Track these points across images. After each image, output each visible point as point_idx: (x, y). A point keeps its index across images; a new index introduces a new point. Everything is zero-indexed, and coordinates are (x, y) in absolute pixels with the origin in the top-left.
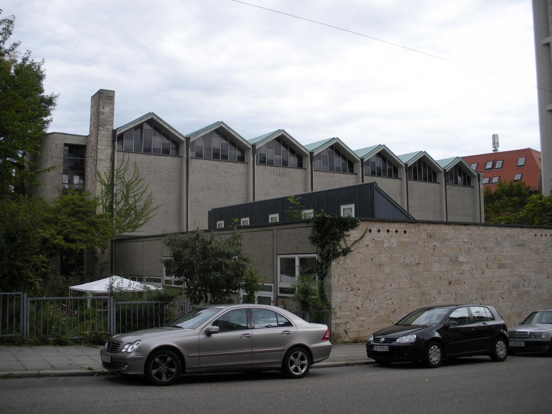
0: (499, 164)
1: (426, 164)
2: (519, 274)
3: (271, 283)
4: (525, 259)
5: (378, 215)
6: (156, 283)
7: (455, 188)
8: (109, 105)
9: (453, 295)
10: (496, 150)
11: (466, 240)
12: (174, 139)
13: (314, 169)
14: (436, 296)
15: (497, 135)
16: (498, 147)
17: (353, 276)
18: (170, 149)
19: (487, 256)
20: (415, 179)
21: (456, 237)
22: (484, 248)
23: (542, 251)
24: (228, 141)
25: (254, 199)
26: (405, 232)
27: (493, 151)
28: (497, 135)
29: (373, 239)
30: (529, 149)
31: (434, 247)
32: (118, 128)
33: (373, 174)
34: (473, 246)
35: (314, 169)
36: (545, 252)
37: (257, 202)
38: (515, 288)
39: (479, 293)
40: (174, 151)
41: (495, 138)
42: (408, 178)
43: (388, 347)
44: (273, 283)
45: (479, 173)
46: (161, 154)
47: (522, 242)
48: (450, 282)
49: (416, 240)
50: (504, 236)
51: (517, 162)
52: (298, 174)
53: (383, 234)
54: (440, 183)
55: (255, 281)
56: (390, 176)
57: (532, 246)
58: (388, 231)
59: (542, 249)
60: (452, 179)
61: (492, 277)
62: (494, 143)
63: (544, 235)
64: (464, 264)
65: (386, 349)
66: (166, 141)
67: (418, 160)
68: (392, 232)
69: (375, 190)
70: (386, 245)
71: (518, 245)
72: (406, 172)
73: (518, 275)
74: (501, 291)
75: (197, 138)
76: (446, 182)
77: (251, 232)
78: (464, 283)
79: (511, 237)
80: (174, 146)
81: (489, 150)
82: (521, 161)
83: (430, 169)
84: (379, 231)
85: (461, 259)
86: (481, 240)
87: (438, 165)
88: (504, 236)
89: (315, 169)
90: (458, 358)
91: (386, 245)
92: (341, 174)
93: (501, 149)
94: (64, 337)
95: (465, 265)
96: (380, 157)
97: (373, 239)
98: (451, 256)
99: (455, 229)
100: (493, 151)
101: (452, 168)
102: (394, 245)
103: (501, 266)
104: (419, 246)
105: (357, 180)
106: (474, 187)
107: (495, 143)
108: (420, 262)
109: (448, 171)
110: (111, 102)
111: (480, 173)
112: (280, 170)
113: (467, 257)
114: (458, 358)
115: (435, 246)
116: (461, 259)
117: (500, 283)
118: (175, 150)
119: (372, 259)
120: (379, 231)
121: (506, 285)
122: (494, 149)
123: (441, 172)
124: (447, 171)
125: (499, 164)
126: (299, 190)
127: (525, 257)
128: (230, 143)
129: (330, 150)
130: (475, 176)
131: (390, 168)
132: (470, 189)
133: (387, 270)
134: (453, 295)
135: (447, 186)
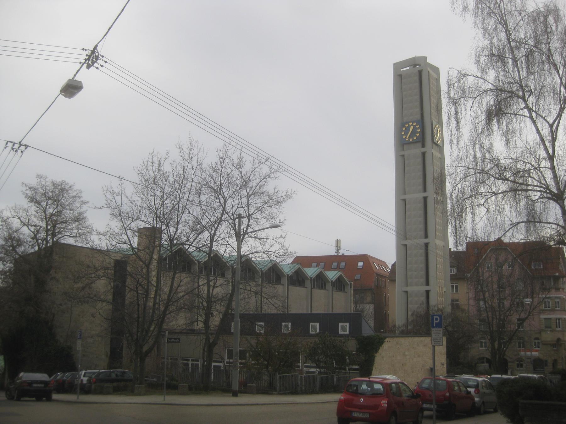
0: (343, 264)
25: (311, 312)
27: (336, 252)
37: (313, 314)
41: (338, 242)
42: (313, 286)
56: (300, 286)
62: (337, 247)
72: (332, 286)
82: (360, 264)
90: (402, 70)
93: (341, 252)
94: (424, 308)
103: (419, 356)
107: (338, 248)
114: (402, 70)
123: (329, 282)
125: (343, 264)
130: (348, 285)
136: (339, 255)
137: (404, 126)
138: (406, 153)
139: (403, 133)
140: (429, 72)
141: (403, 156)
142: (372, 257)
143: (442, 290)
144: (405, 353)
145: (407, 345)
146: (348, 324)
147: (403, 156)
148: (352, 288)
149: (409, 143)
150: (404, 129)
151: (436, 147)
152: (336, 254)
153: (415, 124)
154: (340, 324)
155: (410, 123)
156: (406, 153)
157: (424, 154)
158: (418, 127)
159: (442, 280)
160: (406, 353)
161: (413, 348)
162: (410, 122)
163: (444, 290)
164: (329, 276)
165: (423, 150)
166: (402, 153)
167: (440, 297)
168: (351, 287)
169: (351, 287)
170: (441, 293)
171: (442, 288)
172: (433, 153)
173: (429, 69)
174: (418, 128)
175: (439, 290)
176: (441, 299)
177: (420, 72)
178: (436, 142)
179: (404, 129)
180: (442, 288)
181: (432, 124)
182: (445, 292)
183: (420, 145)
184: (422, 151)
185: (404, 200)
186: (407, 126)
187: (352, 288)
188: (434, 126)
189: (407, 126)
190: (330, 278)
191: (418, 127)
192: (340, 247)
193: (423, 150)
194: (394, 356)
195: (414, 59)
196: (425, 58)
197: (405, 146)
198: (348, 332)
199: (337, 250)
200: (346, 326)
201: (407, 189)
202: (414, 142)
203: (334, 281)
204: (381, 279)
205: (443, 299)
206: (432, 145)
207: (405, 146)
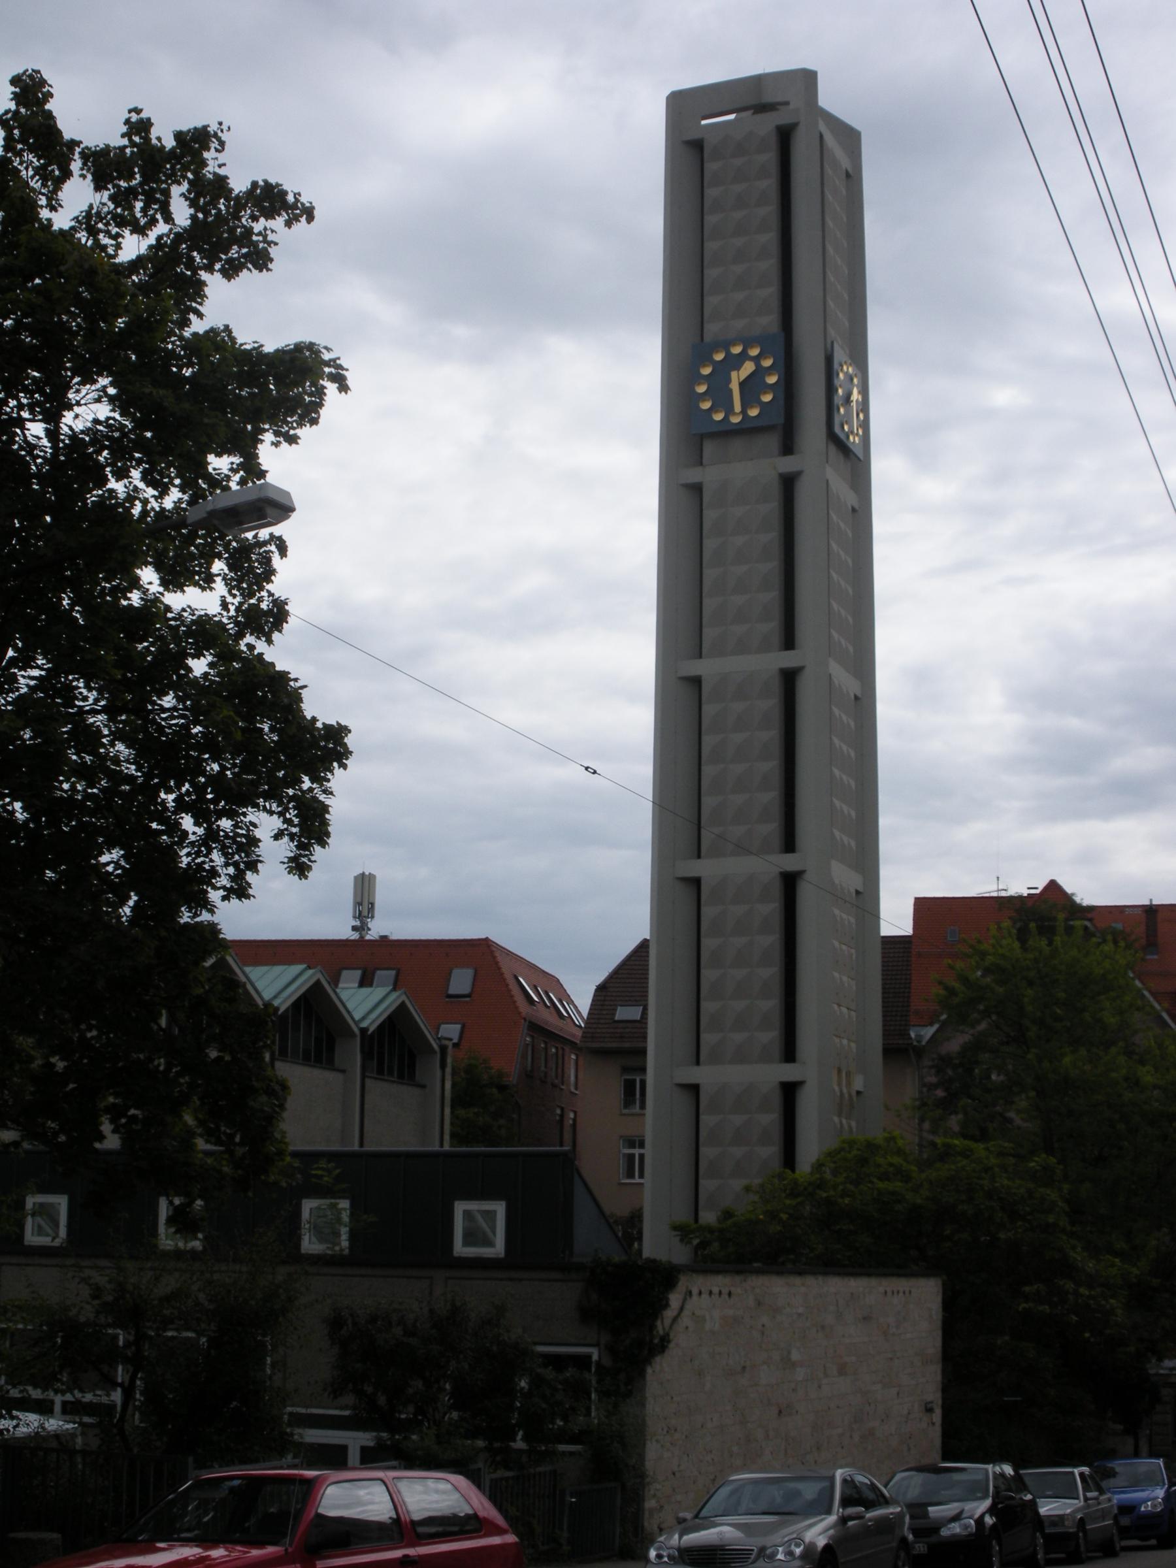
15: (372, 878)
16: (373, 917)
27: (354, 928)
28: (372, 878)
30: (487, 940)
43: (926, 1546)
51: (614, 1014)
62: (358, 903)
65: (922, 1549)
75: (282, 999)
76: (364, 1068)
77: (501, 1280)
87: (349, 1012)
93: (377, 928)
100: (354, 928)
103: (842, 1371)
106: (423, 1087)
107: (364, 906)
109: (374, 1032)
114: (704, 122)
122: (358, 923)
136: (368, 937)
137: (706, 359)
138: (709, 476)
139: (701, 389)
140: (821, 136)
141: (697, 489)
142: (509, 953)
143: (849, 1084)
144: (789, 1353)
145: (800, 1315)
146: (499, 1208)
147: (697, 489)
148: (448, 1070)
149: (727, 433)
150: (706, 371)
151: (841, 457)
152: (355, 936)
153: (754, 352)
154: (460, 1208)
155: (734, 345)
156: (709, 476)
157: (789, 483)
158: (767, 363)
159: (849, 1040)
160: (795, 1356)
161: (823, 1327)
162: (733, 343)
163: (858, 1083)
164: (350, 1006)
165: (787, 464)
166: (693, 475)
167: (840, 1115)
168: (443, 1066)
169: (443, 1066)
170: (846, 1096)
171: (848, 1074)
172: (827, 481)
173: (822, 127)
174: (769, 371)
175: (839, 1084)
176: (844, 1121)
177: (785, 136)
178: (842, 436)
179: (706, 371)
180: (848, 1074)
181: (829, 360)
182: (858, 1093)
183: (773, 442)
184: (780, 471)
185: (696, 682)
186: (719, 357)
187: (448, 1070)
188: (836, 366)
189: (719, 357)
190: (357, 1017)
191: (767, 363)
192: (373, 904)
193: (787, 464)
194: (744, 1368)
195: (757, 82)
196: (807, 79)
197: (709, 447)
198: (498, 1248)
199: (360, 916)
200: (490, 1216)
201: (709, 633)
202: (748, 430)
203: (372, 1029)
204: (546, 1049)
205: (853, 1124)
206: (827, 447)
207: (709, 447)
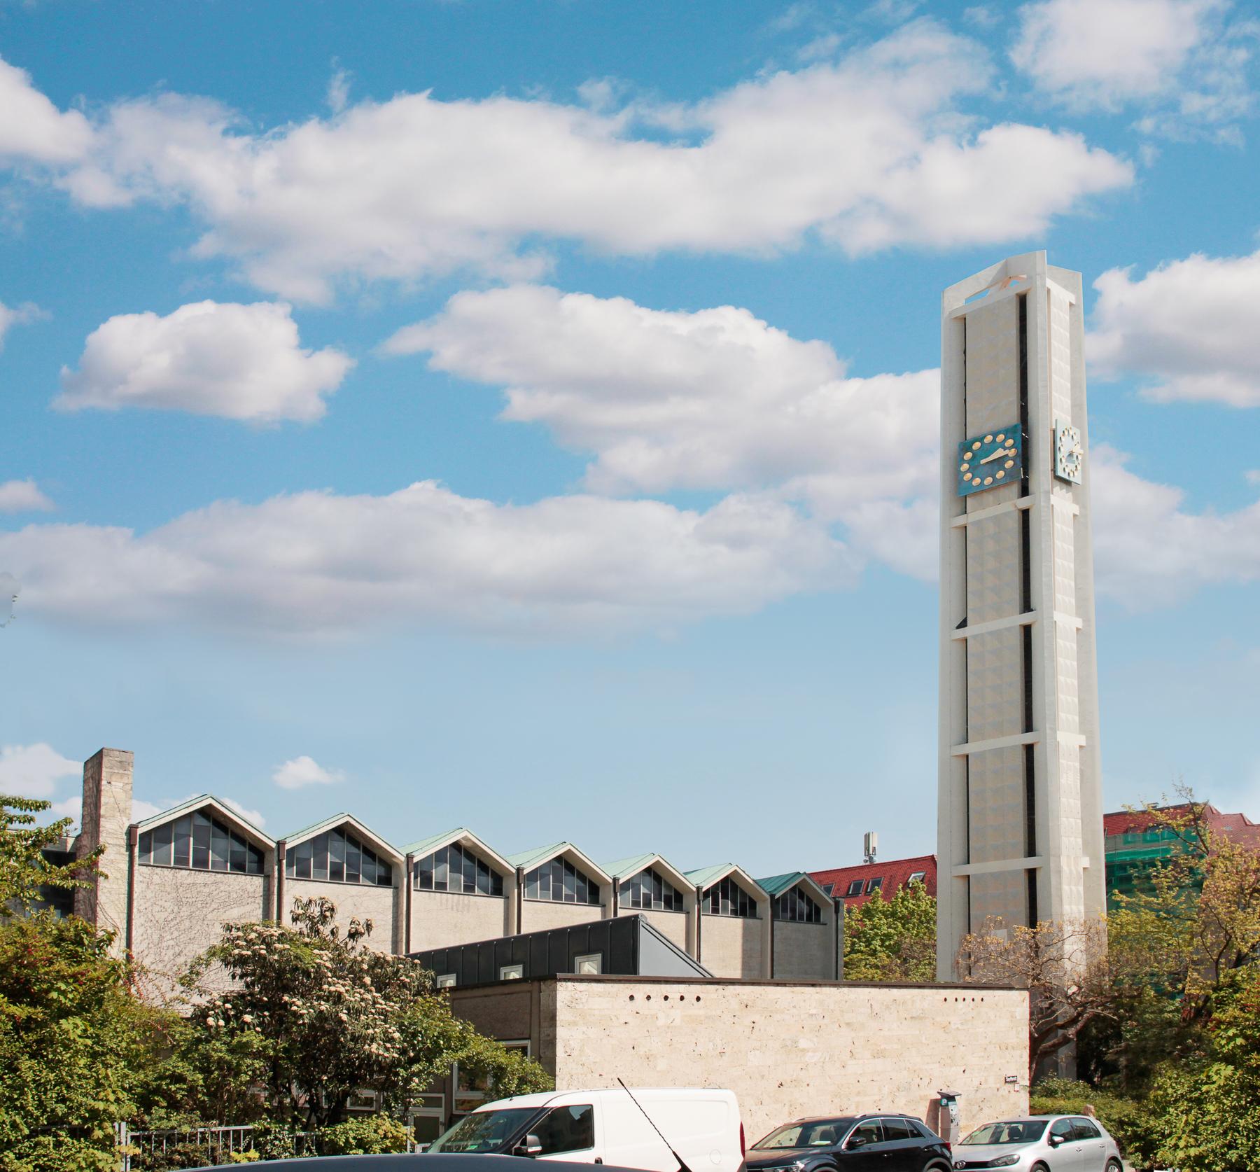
1: (737, 886)
2: (911, 1068)
3: (439, 1093)
4: (924, 1041)
5: (643, 971)
6: (1151, 893)
7: (792, 926)
8: (122, 778)
9: (787, 1107)
10: (871, 859)
11: (813, 1011)
12: (252, 843)
13: (524, 897)
14: (754, 1108)
17: (597, 1076)
18: (245, 861)
19: (853, 1038)
20: (715, 911)
21: (794, 1007)
22: (848, 1024)
23: (957, 1026)
24: (359, 849)
26: (698, 999)
29: (637, 1013)
31: (753, 1025)
32: (139, 823)
33: (636, 904)
34: (826, 1021)
35: (524, 897)
36: (960, 1028)
38: (902, 1091)
39: (836, 1101)
40: (255, 866)
44: (444, 1092)
45: (837, 899)
46: (229, 871)
47: (921, 1011)
48: (781, 1085)
49: (719, 1013)
50: (885, 1003)
52: (496, 905)
53: (657, 1001)
54: (762, 919)
55: (40, 832)
57: (938, 1019)
58: (666, 998)
59: (955, 1024)
60: (785, 910)
61: (861, 1074)
63: (978, 999)
64: (808, 1051)
66: (238, 847)
67: (712, 887)
68: (673, 999)
69: (642, 929)
70: (661, 1022)
71: (912, 1018)
73: (909, 1068)
74: (877, 1098)
76: (774, 916)
78: (808, 1085)
79: (899, 1005)
80: (255, 858)
81: (858, 860)
83: (743, 894)
84: (649, 998)
85: (803, 1044)
86: (843, 1011)
88: (885, 1003)
89: (526, 899)
91: (661, 1022)
92: (575, 906)
95: (810, 1054)
96: (650, 875)
97: (637, 1013)
98: (784, 1040)
99: (793, 992)
101: (787, 892)
102: (678, 1022)
103: (879, 1054)
104: (725, 1023)
105: (604, 914)
108: (724, 1050)
110: (126, 772)
111: (840, 899)
112: (463, 900)
113: (815, 1039)
115: (754, 1023)
116: (803, 1044)
117: (874, 1083)
118: (256, 864)
119: (633, 1048)
120: (649, 998)
121: (887, 1086)
124: (776, 897)
126: (495, 932)
127: (924, 1038)
128: (363, 852)
129: (557, 864)
131: (668, 893)
132: (819, 927)
133: (662, 1065)
134: (787, 1107)
135: (775, 922)
